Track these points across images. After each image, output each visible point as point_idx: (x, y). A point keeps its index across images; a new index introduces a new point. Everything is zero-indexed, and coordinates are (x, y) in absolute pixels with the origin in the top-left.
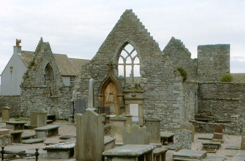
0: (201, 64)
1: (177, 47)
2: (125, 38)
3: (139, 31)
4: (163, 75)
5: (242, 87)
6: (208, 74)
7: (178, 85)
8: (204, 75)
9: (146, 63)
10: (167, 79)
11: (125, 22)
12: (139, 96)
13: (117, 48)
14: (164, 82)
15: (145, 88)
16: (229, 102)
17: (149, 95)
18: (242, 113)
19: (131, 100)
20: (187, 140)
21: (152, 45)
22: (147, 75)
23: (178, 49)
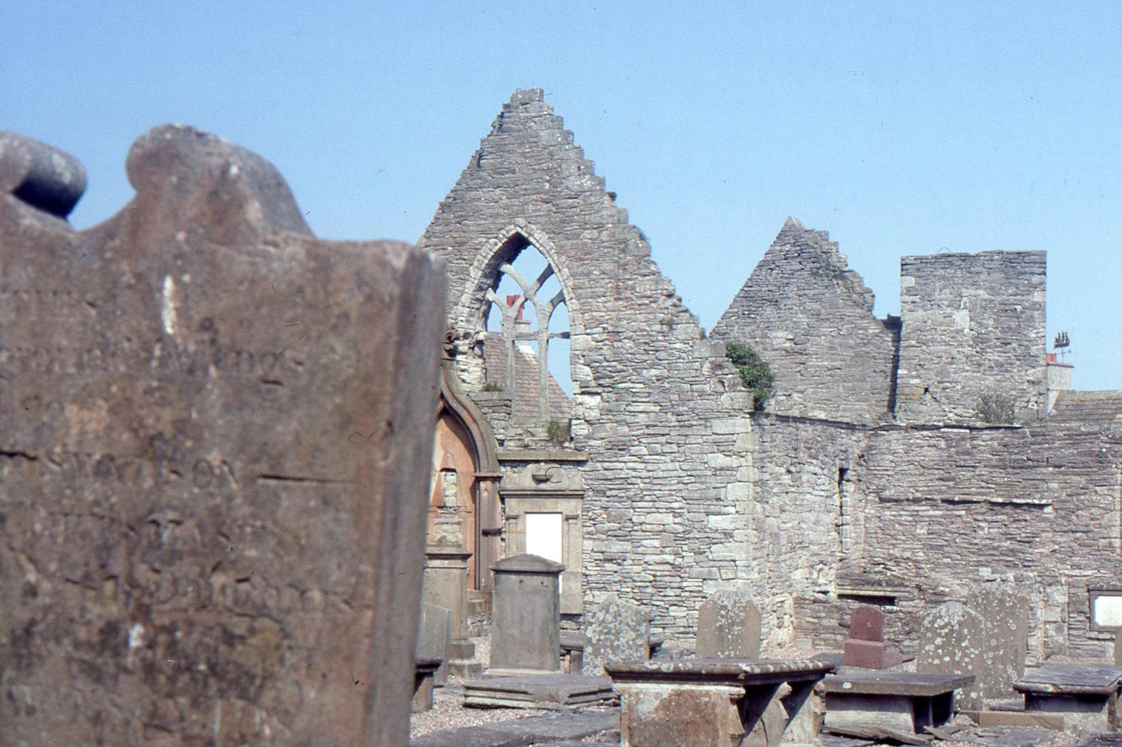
0: (913, 342)
1: (812, 265)
2: (512, 216)
3: (567, 188)
4: (666, 384)
5: (1057, 444)
6: (944, 389)
7: (729, 430)
8: (928, 396)
9: (596, 330)
10: (683, 402)
11: (510, 147)
12: (569, 478)
13: (476, 263)
14: (669, 415)
15: (592, 443)
16: (1000, 517)
17: (609, 474)
18: (1059, 566)
19: (532, 496)
20: (630, 647)
21: (622, 246)
22: (600, 385)
23: (814, 274)
